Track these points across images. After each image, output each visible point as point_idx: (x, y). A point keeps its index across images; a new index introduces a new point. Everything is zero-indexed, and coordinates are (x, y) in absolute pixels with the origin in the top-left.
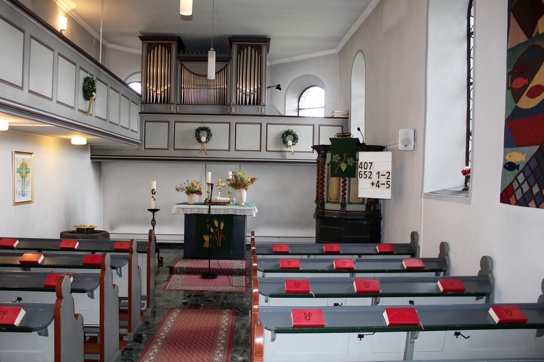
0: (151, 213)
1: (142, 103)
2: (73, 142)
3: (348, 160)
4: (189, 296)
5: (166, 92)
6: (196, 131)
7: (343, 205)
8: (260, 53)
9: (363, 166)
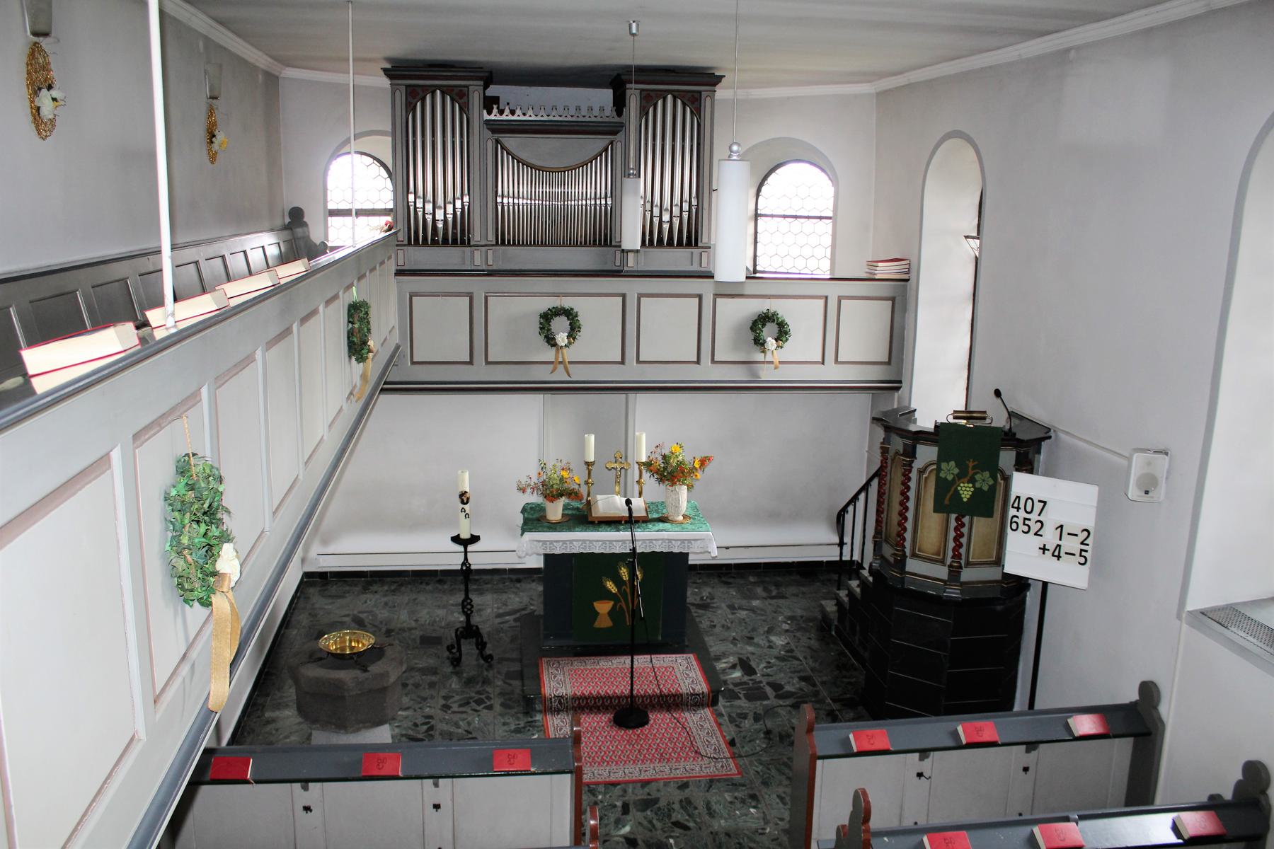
3: (978, 477)
8: (697, 112)
9: (1022, 506)
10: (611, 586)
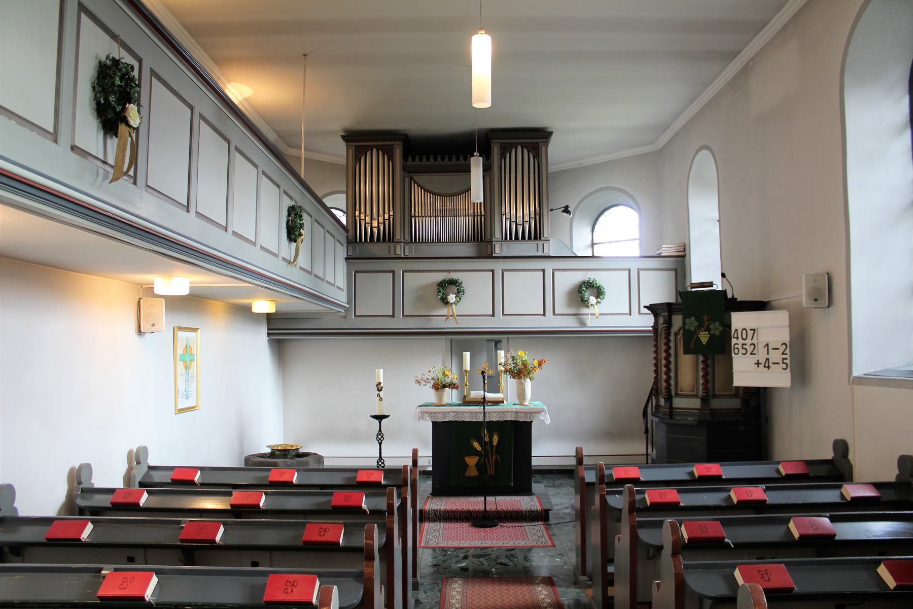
0: (377, 422)
1: (349, 242)
2: (255, 309)
3: (712, 326)
4: (466, 557)
5: (387, 223)
7: (705, 400)
8: (537, 156)
9: (740, 336)
10: (476, 445)
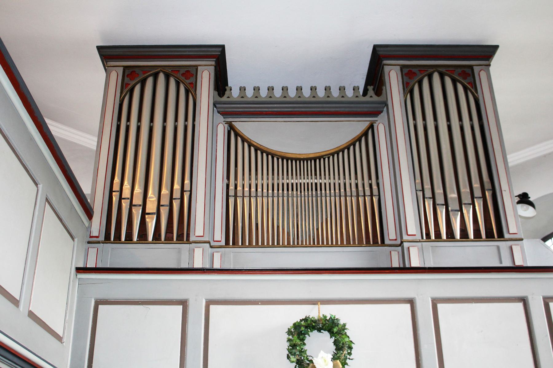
6: (289, 332)
